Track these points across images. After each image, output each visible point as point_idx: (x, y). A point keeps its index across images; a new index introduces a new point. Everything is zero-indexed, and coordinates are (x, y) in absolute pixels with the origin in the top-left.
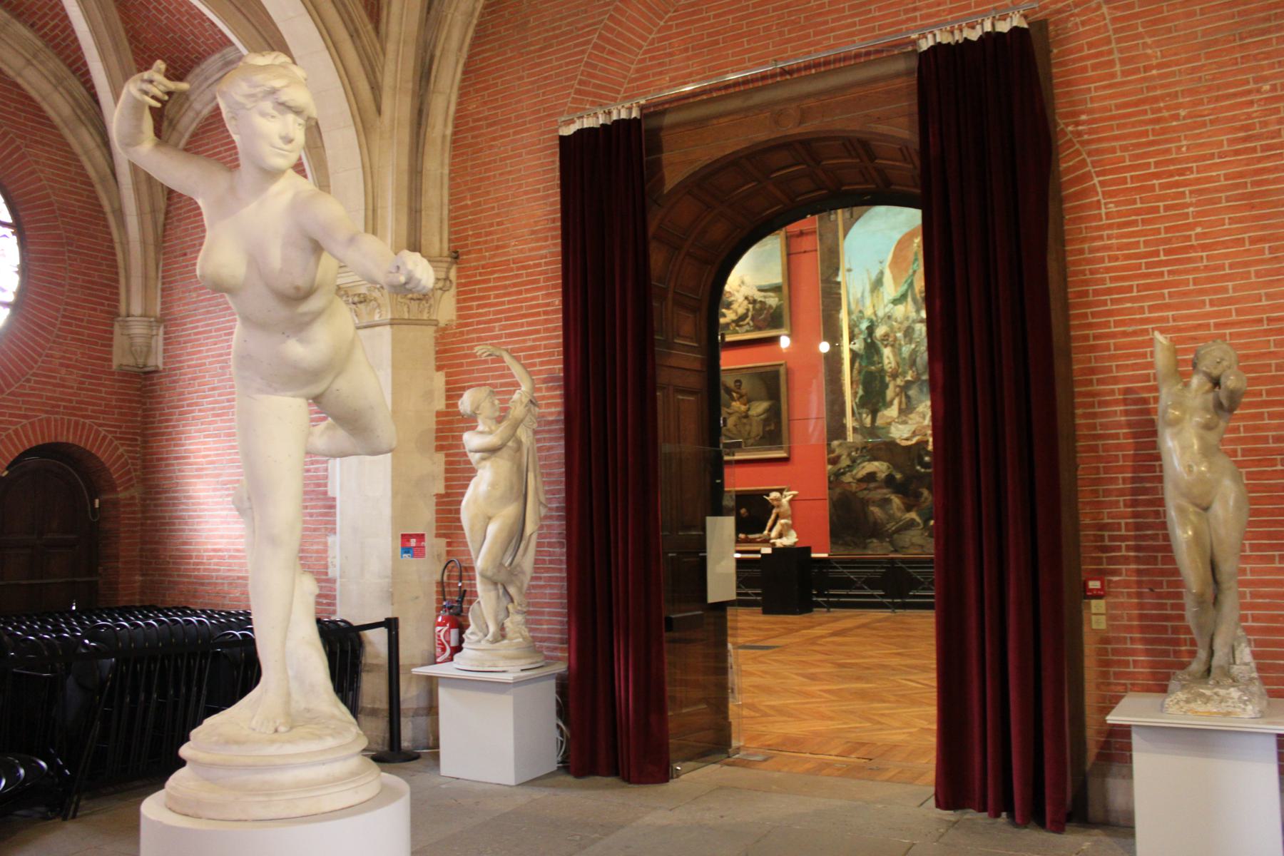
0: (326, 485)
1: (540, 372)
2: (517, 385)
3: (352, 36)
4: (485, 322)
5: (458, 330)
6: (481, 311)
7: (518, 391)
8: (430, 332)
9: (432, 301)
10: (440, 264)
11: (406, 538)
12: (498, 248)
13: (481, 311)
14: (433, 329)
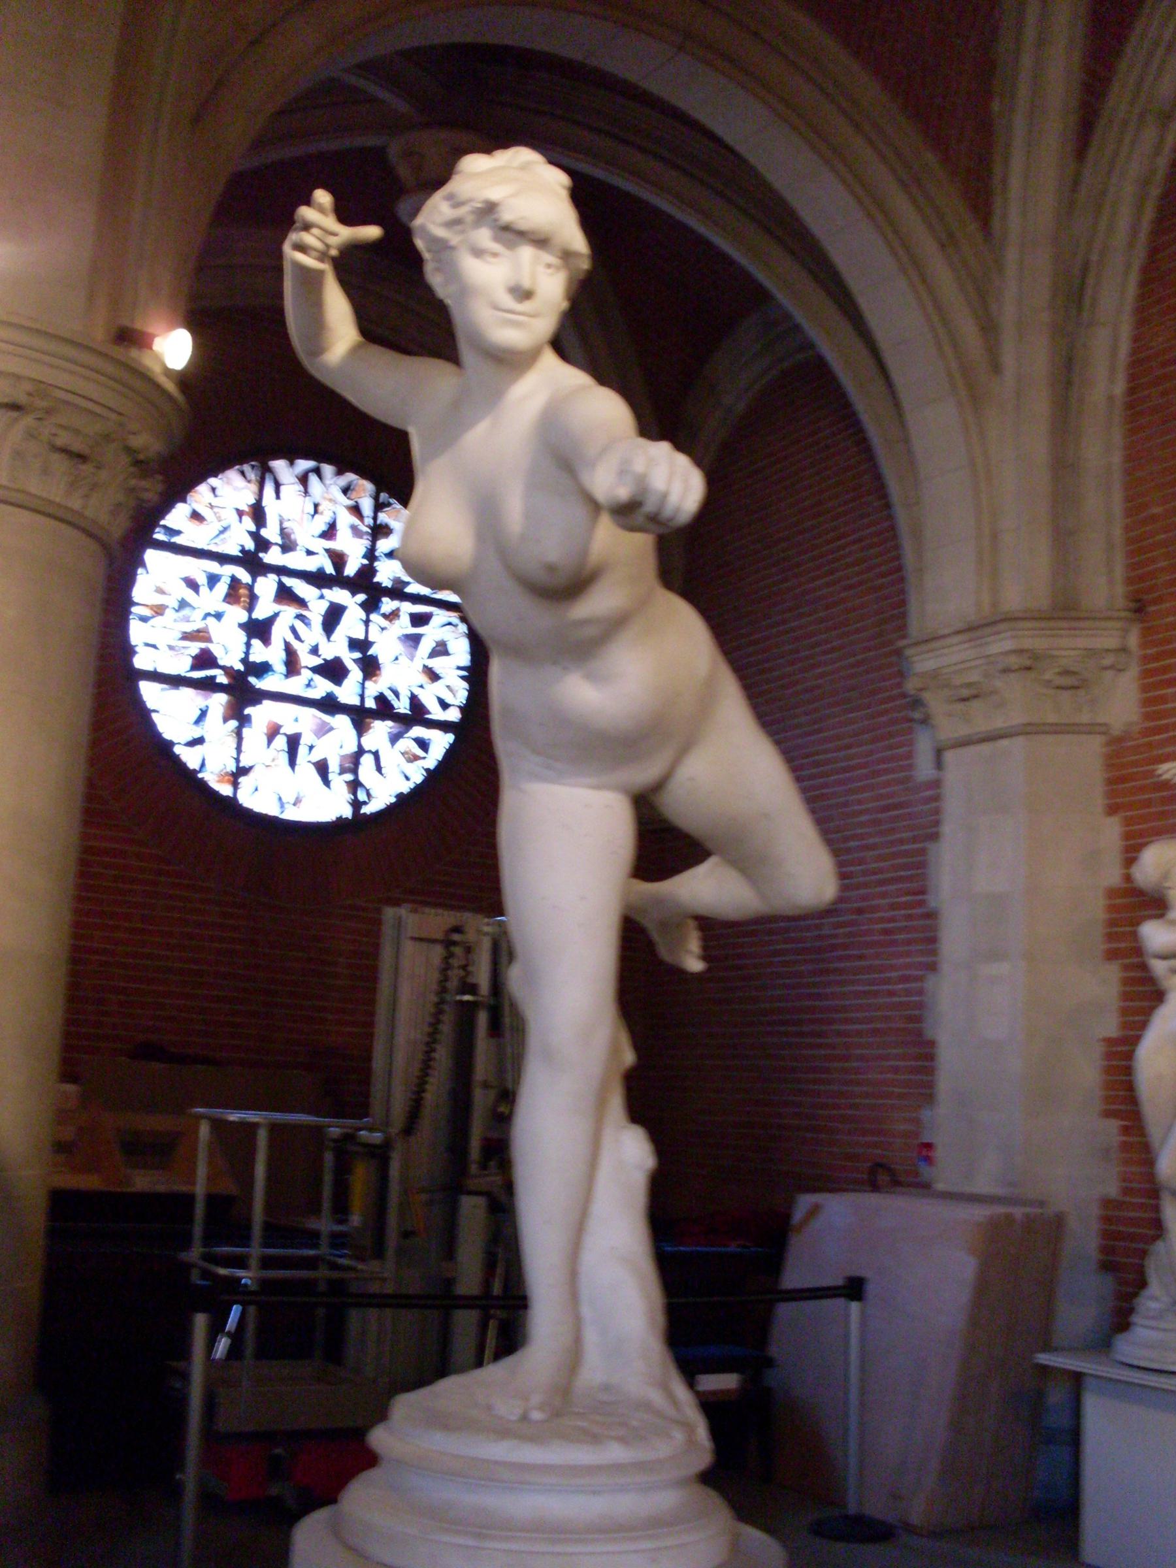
8: (1095, 745)
10: (1110, 624)
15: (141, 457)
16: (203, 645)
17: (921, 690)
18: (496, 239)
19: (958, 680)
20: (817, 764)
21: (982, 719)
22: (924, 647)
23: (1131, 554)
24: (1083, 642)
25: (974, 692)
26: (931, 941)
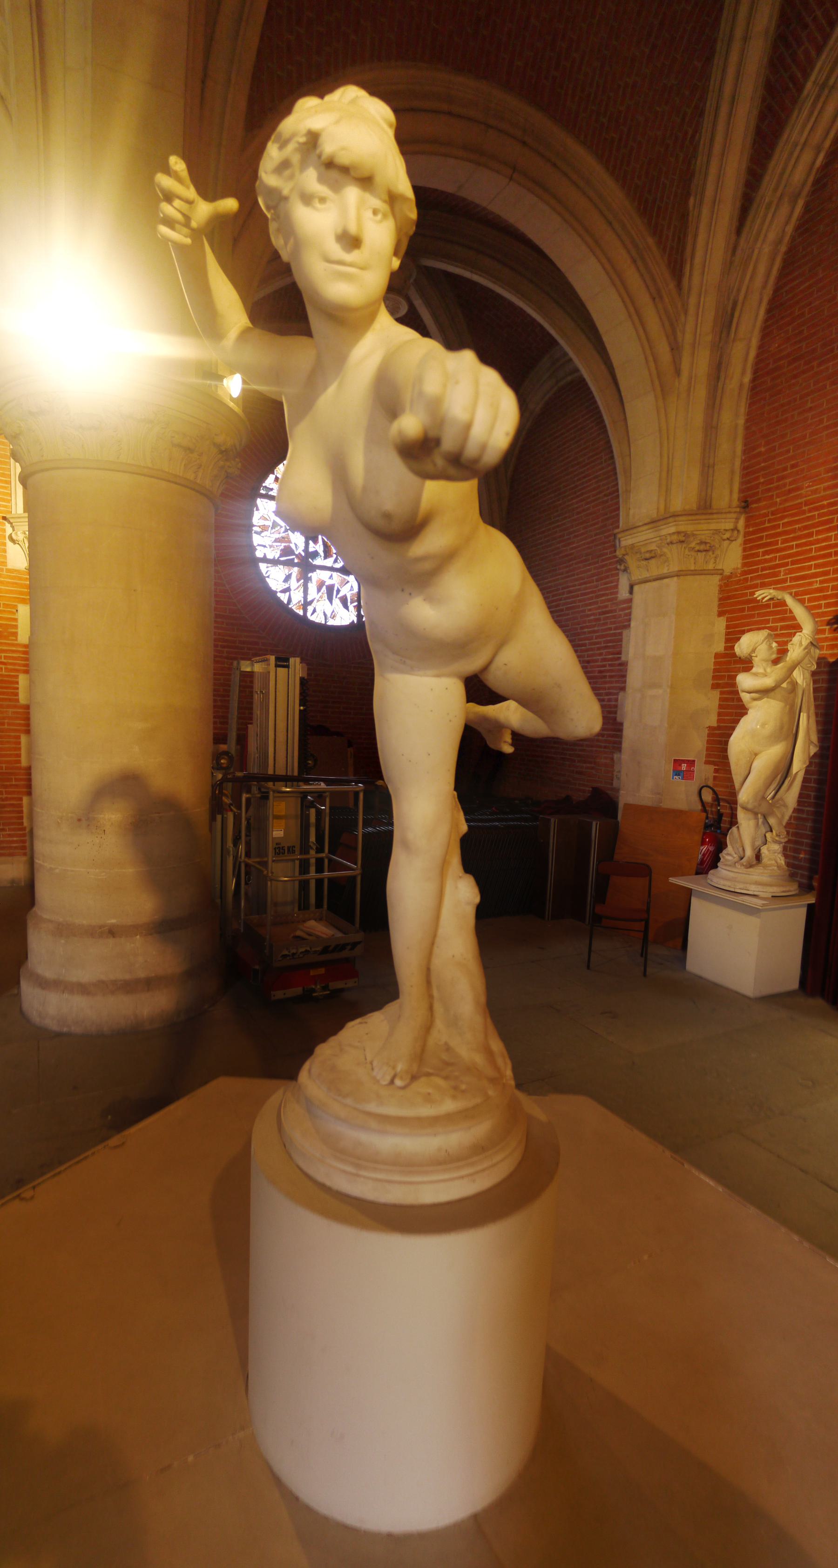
0: (616, 713)
1: (824, 614)
2: (798, 628)
3: (654, 299)
4: (770, 568)
5: (742, 578)
6: (767, 557)
7: (798, 634)
8: (716, 579)
9: (718, 552)
10: (729, 516)
11: (677, 762)
12: (790, 491)
13: (767, 557)
14: (718, 577)
15: (223, 448)
16: (287, 544)
17: (624, 555)
18: (321, 180)
19: (643, 550)
20: (570, 592)
21: (655, 568)
22: (627, 533)
23: (744, 476)
24: (713, 526)
25: (653, 555)
26: (623, 677)
